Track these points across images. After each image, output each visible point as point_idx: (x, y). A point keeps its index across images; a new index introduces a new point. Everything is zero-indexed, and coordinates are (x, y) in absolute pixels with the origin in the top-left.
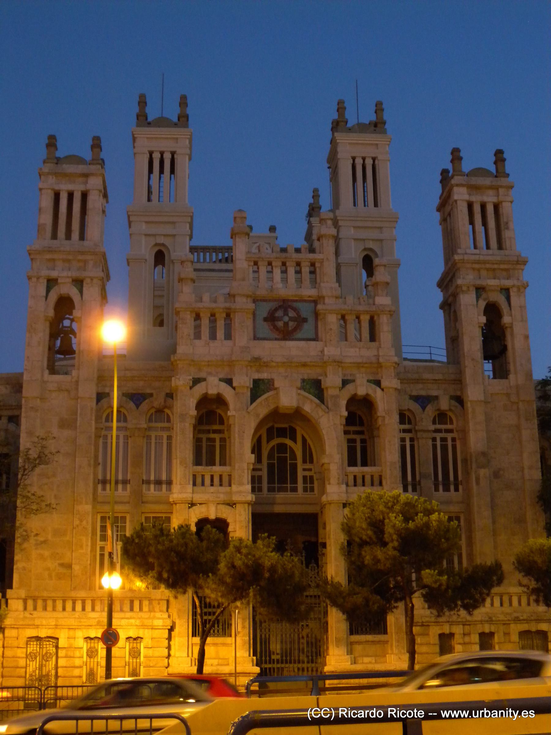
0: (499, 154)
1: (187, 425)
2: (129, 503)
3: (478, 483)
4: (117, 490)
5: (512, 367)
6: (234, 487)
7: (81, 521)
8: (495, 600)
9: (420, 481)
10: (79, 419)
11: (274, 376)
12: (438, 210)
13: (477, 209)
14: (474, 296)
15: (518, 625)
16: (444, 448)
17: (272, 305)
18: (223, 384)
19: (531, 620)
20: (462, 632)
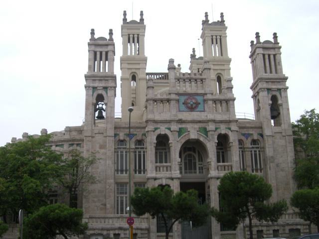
0: (275, 34)
1: (153, 147)
3: (270, 169)
5: (282, 122)
6: (173, 172)
7: (110, 186)
12: (250, 57)
13: (267, 57)
14: (266, 92)
16: (256, 155)
18: (167, 130)
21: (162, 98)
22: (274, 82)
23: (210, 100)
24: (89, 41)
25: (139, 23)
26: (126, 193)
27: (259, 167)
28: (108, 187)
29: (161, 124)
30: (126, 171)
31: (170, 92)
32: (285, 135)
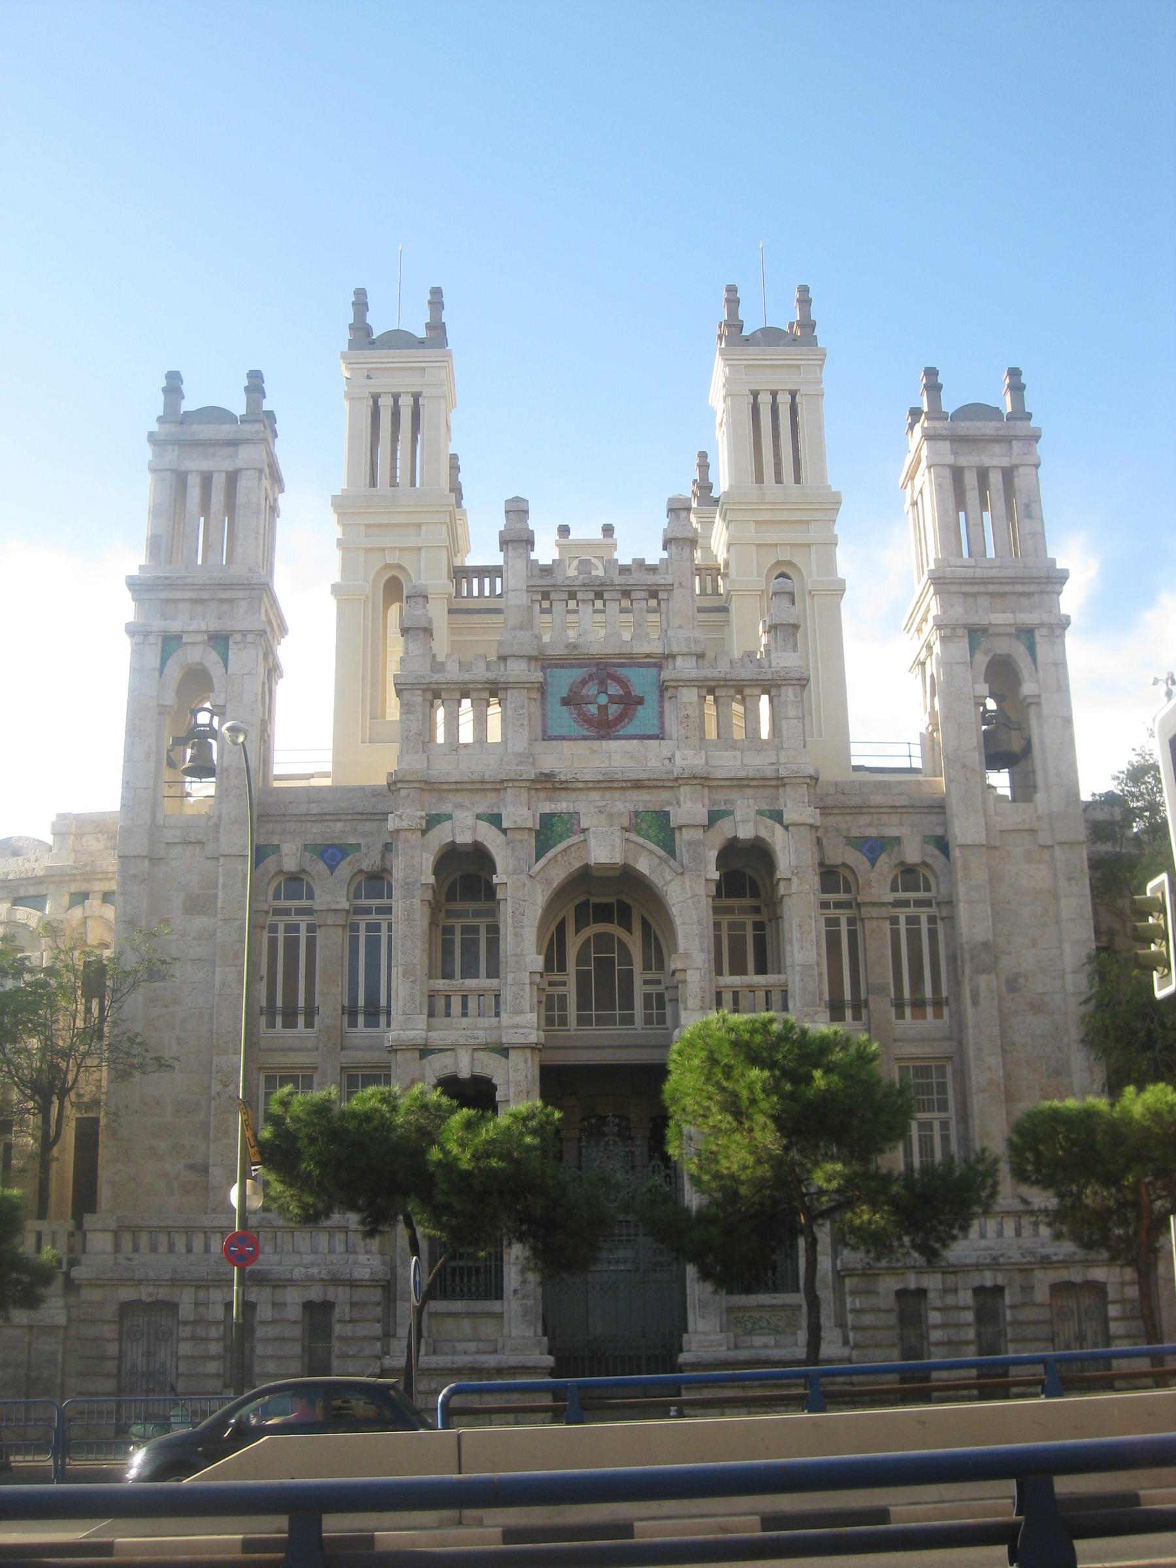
1: (417, 902)
2: (895, 1040)
3: (975, 1003)
4: (356, 1026)
6: (505, 1018)
7: (226, 1086)
8: (1005, 1226)
9: (866, 1001)
10: (221, 895)
11: (582, 808)
15: (1049, 1272)
16: (914, 936)
17: (579, 673)
18: (484, 826)
19: (1074, 1262)
20: (940, 1286)
21: (466, 677)
22: (1004, 595)
23: (690, 683)
24: (155, 427)
25: (421, 343)
26: (943, 1106)
27: (928, 993)
28: (216, 1087)
29: (458, 798)
30: (938, 1004)
31: (504, 652)
32: (1049, 843)
